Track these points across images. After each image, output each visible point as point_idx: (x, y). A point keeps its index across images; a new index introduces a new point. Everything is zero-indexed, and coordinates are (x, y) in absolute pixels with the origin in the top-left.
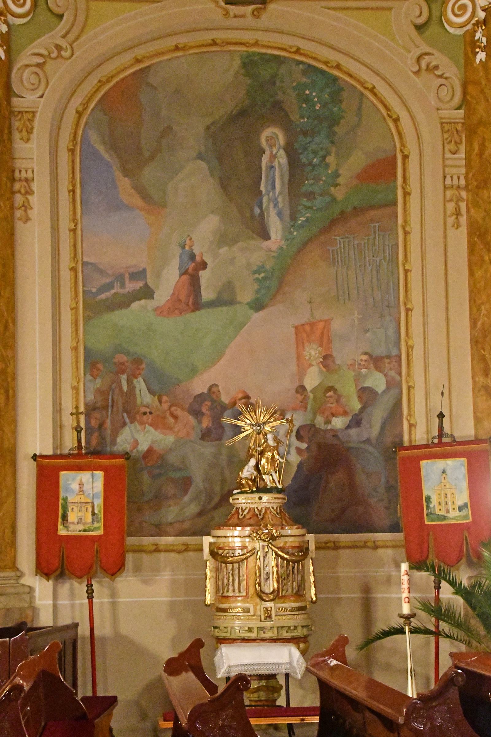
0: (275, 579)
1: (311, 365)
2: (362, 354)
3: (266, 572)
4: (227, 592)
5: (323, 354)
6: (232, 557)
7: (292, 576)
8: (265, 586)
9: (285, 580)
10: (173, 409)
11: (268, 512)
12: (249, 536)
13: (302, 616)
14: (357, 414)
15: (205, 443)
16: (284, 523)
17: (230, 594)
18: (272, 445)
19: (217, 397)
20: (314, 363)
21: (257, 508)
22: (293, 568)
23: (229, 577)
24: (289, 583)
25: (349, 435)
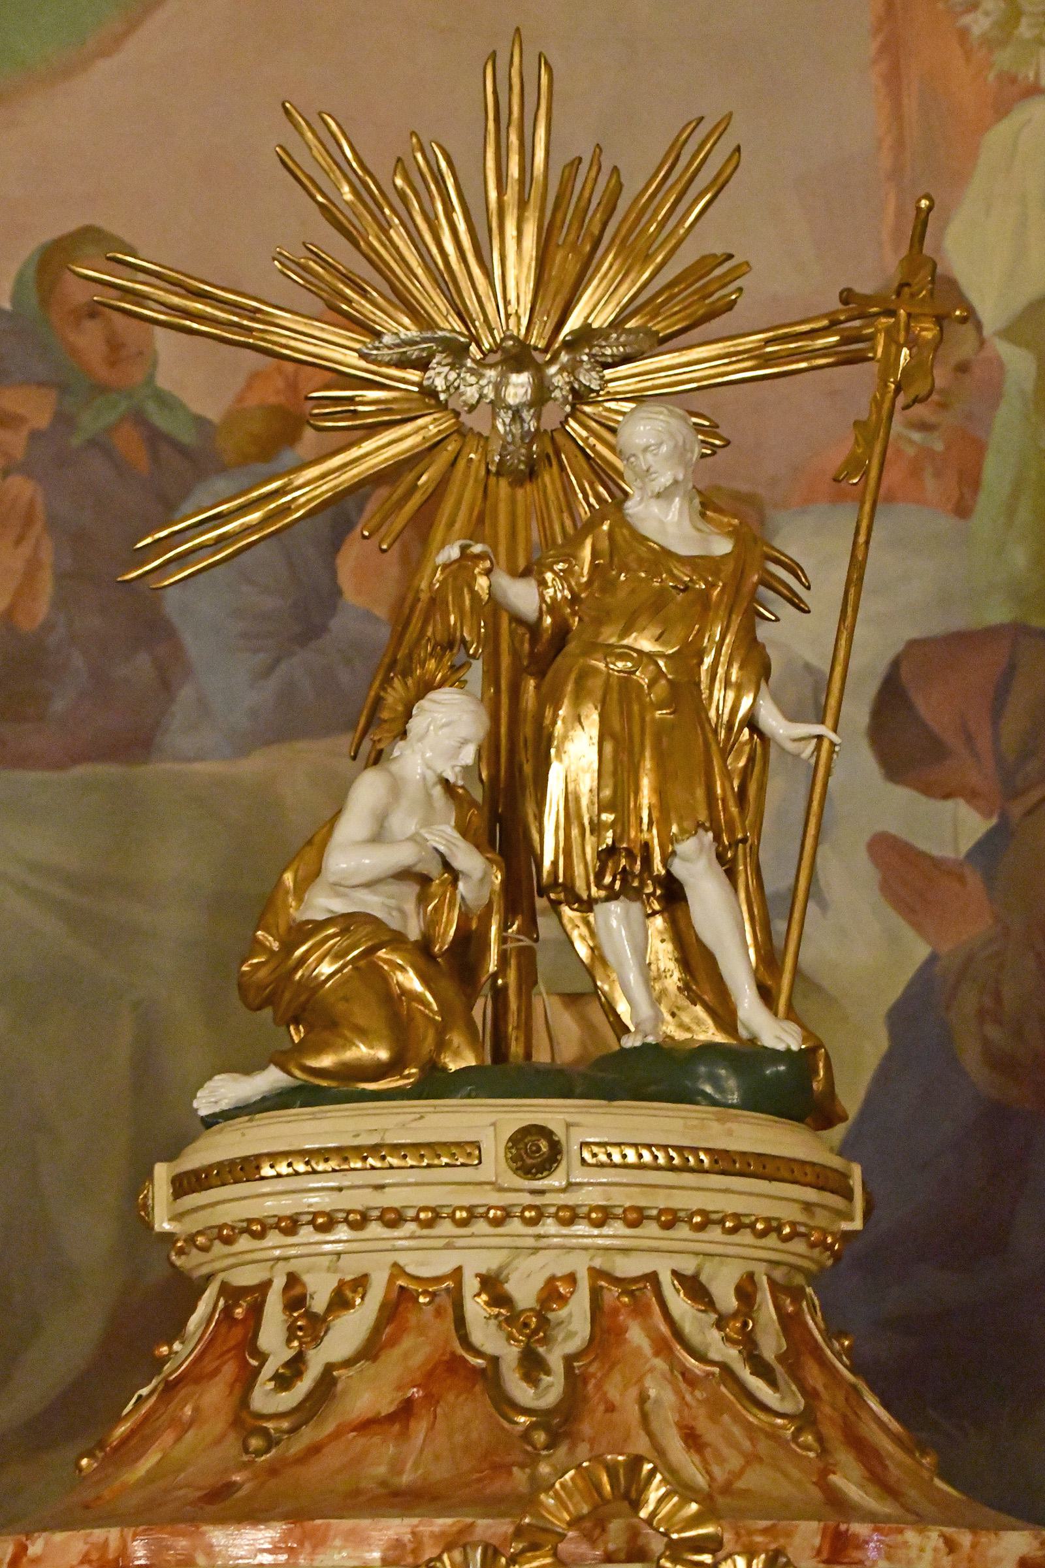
11: (636, 1335)
18: (683, 549)
19: (115, 346)
21: (491, 1284)
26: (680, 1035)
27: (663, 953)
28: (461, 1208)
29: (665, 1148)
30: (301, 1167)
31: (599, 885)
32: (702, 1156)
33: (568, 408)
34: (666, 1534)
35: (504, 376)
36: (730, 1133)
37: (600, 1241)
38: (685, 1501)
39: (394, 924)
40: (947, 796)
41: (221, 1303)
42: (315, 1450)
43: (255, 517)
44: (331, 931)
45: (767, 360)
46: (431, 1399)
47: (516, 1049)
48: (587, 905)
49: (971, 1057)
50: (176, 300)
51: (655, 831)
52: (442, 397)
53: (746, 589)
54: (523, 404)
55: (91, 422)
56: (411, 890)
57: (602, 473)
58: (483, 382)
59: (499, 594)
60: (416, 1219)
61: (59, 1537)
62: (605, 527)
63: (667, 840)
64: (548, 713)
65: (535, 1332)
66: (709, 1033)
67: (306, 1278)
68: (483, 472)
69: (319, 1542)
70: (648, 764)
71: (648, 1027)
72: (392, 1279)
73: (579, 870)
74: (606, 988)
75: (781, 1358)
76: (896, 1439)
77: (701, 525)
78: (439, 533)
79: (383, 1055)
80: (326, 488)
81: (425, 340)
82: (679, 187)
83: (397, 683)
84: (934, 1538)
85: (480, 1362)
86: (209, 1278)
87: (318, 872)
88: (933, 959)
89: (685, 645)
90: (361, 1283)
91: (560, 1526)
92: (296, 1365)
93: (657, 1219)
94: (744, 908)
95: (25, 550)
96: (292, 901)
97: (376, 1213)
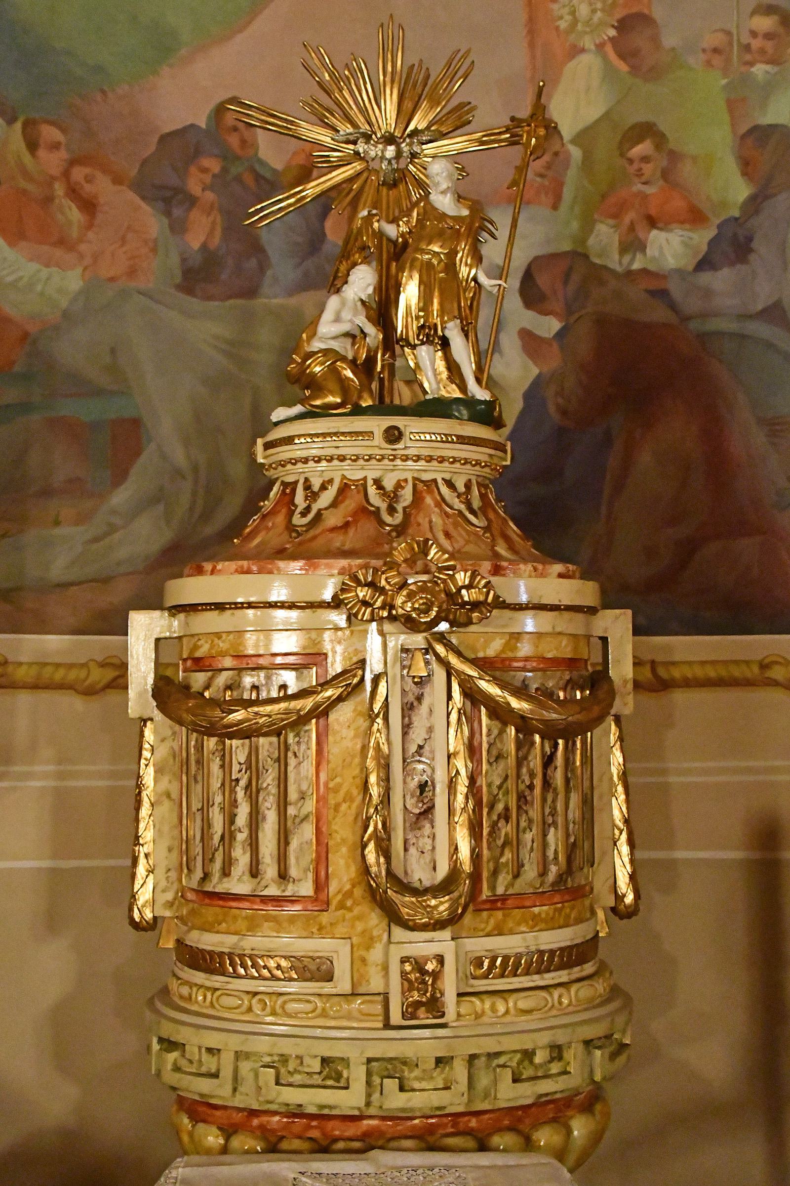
0: (461, 819)
1: (576, 51)
2: (754, 13)
3: (413, 784)
4: (226, 873)
5: (619, 14)
6: (251, 703)
7: (544, 800)
8: (413, 850)
9: (507, 820)
10: (78, 173)
11: (429, 500)
12: (336, 603)
13: (584, 991)
14: (736, 219)
15: (194, 304)
16: (501, 550)
17: (239, 884)
18: (451, 213)
19: (243, 142)
20: (588, 42)
21: (378, 483)
22: (548, 761)
23: (234, 803)
24: (528, 836)
25: (708, 293)
26: (447, 395)
27: (441, 365)
28: (367, 455)
29: (440, 434)
30: (309, 440)
31: (418, 339)
32: (453, 437)
33: (409, 160)
34: (436, 565)
35: (385, 147)
36: (463, 429)
37: (416, 468)
38: (444, 553)
39: (343, 352)
40: (546, 315)
41: (282, 488)
42: (314, 538)
43: (292, 200)
44: (320, 355)
45: (482, 143)
46: (356, 521)
47: (387, 400)
48: (414, 347)
49: (552, 409)
50: (263, 118)
51: (439, 319)
52: (362, 155)
53: (474, 229)
54: (392, 158)
55: (235, 170)
56: (349, 341)
57: (420, 184)
58: (377, 149)
59: (381, 227)
60: (350, 459)
61: (227, 563)
62: (422, 204)
63: (443, 323)
64: (400, 275)
65: (393, 498)
66: (457, 394)
67: (311, 479)
68: (377, 184)
69: (316, 567)
70: (436, 294)
71: (435, 392)
72: (342, 481)
73: (411, 334)
74: (420, 378)
75: (480, 508)
76: (518, 535)
77: (459, 205)
78: (361, 205)
79: (339, 400)
80: (318, 190)
81: (355, 133)
82: (451, 76)
83: (344, 263)
84: (529, 567)
85: (373, 509)
86: (277, 479)
87: (315, 334)
88: (539, 377)
89: (451, 249)
90: (331, 481)
91: (400, 561)
92: (308, 509)
93: (437, 460)
94: (471, 349)
95: (211, 218)
96: (305, 344)
97: (336, 457)
